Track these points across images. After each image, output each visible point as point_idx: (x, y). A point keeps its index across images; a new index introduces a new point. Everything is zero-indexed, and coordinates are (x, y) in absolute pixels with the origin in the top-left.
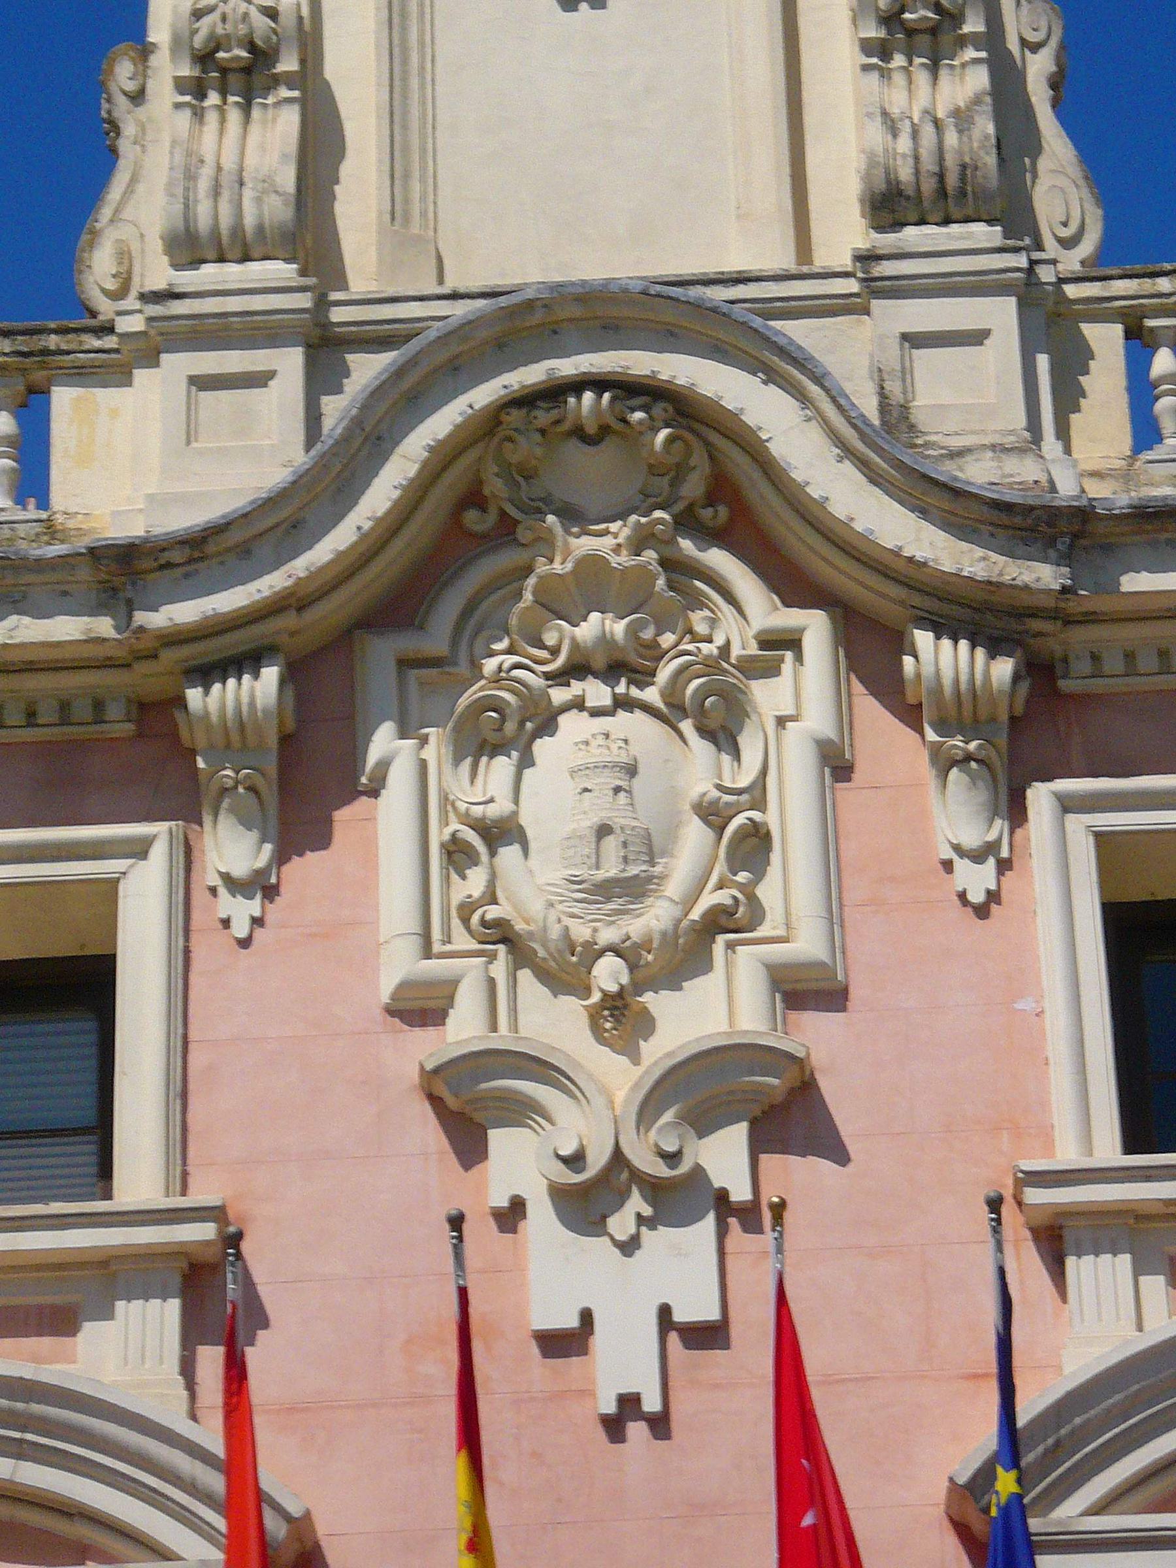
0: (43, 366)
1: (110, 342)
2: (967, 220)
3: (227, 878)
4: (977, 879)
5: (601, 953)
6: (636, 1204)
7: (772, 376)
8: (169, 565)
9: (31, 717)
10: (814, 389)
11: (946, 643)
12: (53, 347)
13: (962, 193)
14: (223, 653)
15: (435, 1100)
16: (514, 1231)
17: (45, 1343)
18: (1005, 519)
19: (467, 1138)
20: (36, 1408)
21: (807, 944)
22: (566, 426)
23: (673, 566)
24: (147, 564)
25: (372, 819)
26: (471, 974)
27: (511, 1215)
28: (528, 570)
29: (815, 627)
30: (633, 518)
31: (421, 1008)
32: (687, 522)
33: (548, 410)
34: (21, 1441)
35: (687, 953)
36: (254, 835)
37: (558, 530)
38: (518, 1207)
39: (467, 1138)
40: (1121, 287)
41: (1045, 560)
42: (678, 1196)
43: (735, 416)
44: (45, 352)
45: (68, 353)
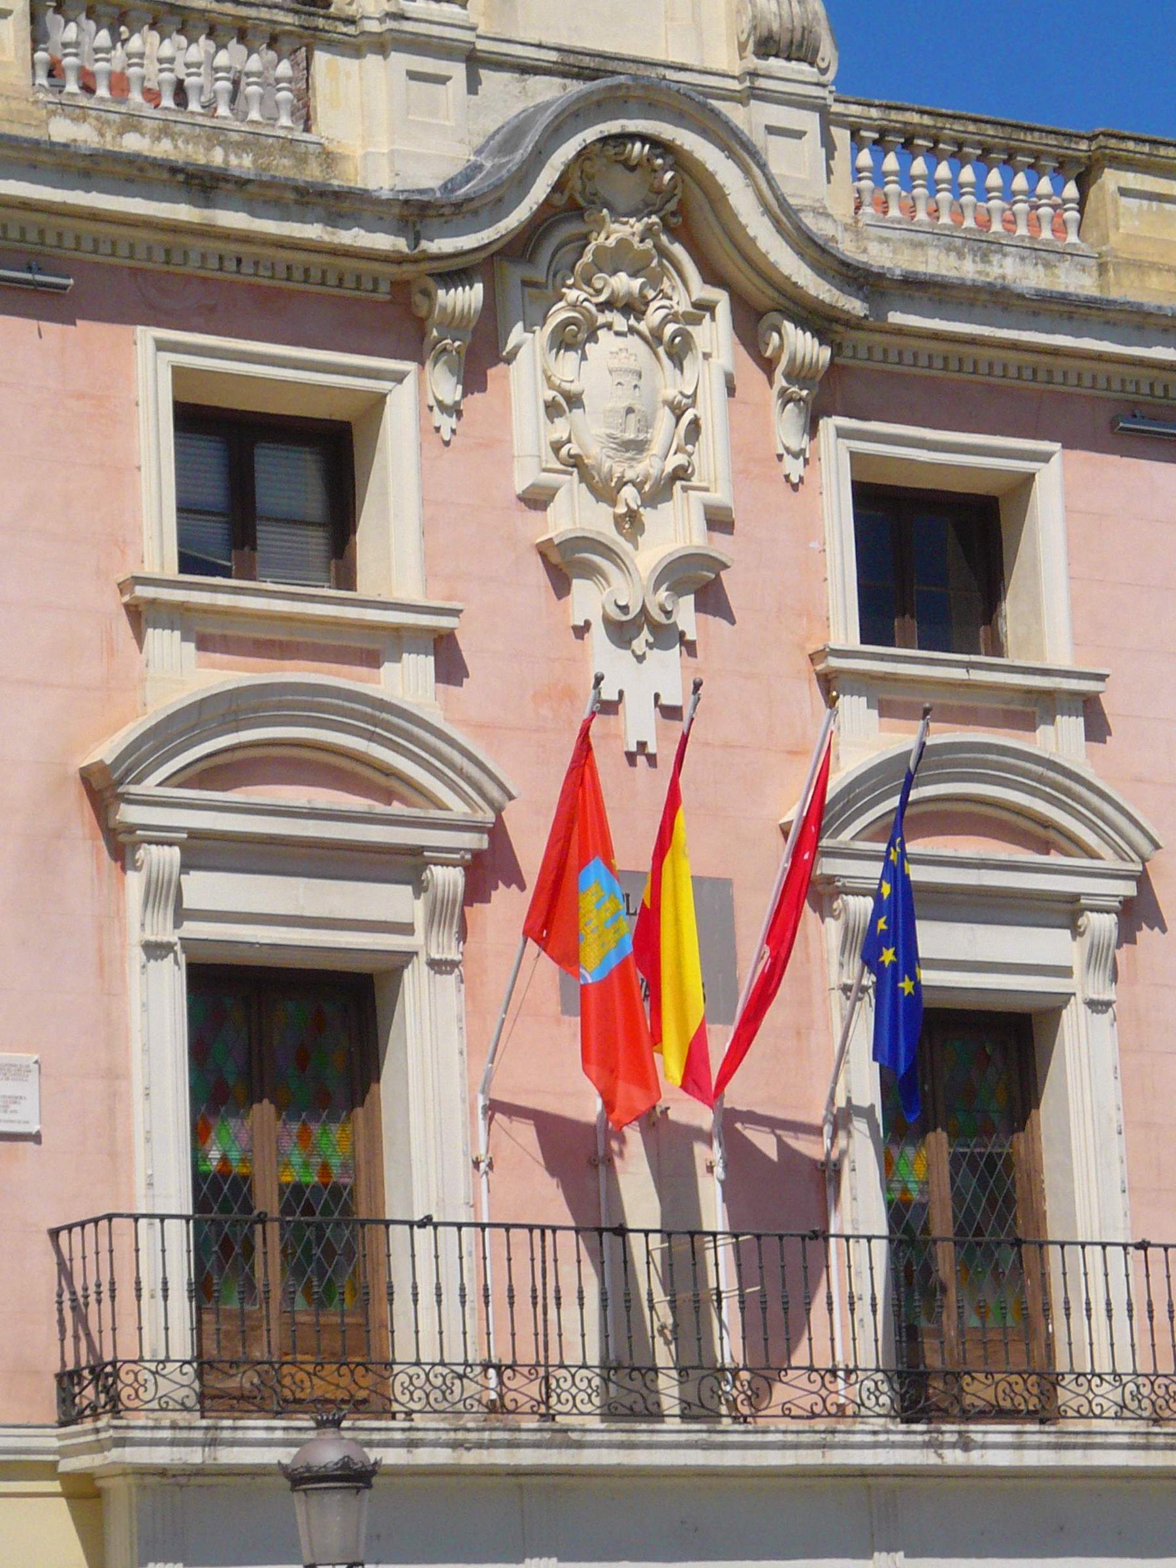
0: (313, 37)
1: (351, 30)
2: (799, 60)
3: (440, 403)
4: (794, 468)
5: (626, 484)
6: (646, 635)
7: (732, 155)
8: (442, 215)
9: (340, 285)
10: (756, 170)
11: (800, 332)
12: (321, 27)
13: (801, 45)
14: (456, 272)
15: (544, 556)
16: (583, 639)
17: (364, 671)
18: (844, 270)
19: (560, 582)
20: (385, 716)
21: (720, 496)
22: (622, 158)
23: (663, 253)
24: (431, 212)
25: (506, 377)
26: (570, 488)
27: (581, 631)
28: (585, 239)
29: (722, 299)
30: (646, 219)
31: (537, 500)
32: (668, 229)
33: (615, 147)
34: (374, 732)
35: (659, 491)
36: (454, 380)
37: (608, 219)
38: (587, 625)
39: (560, 582)
40: (854, 109)
41: (857, 297)
42: (667, 636)
43: (711, 176)
44: (316, 29)
45: (329, 32)
